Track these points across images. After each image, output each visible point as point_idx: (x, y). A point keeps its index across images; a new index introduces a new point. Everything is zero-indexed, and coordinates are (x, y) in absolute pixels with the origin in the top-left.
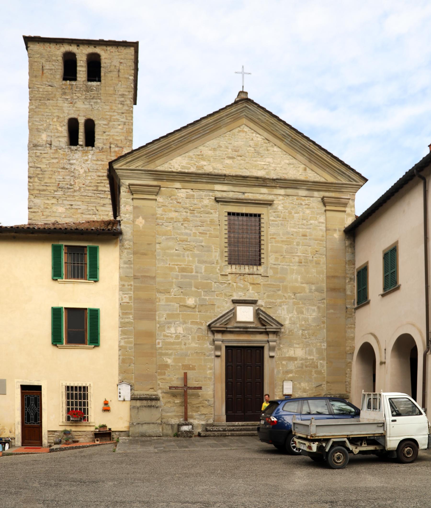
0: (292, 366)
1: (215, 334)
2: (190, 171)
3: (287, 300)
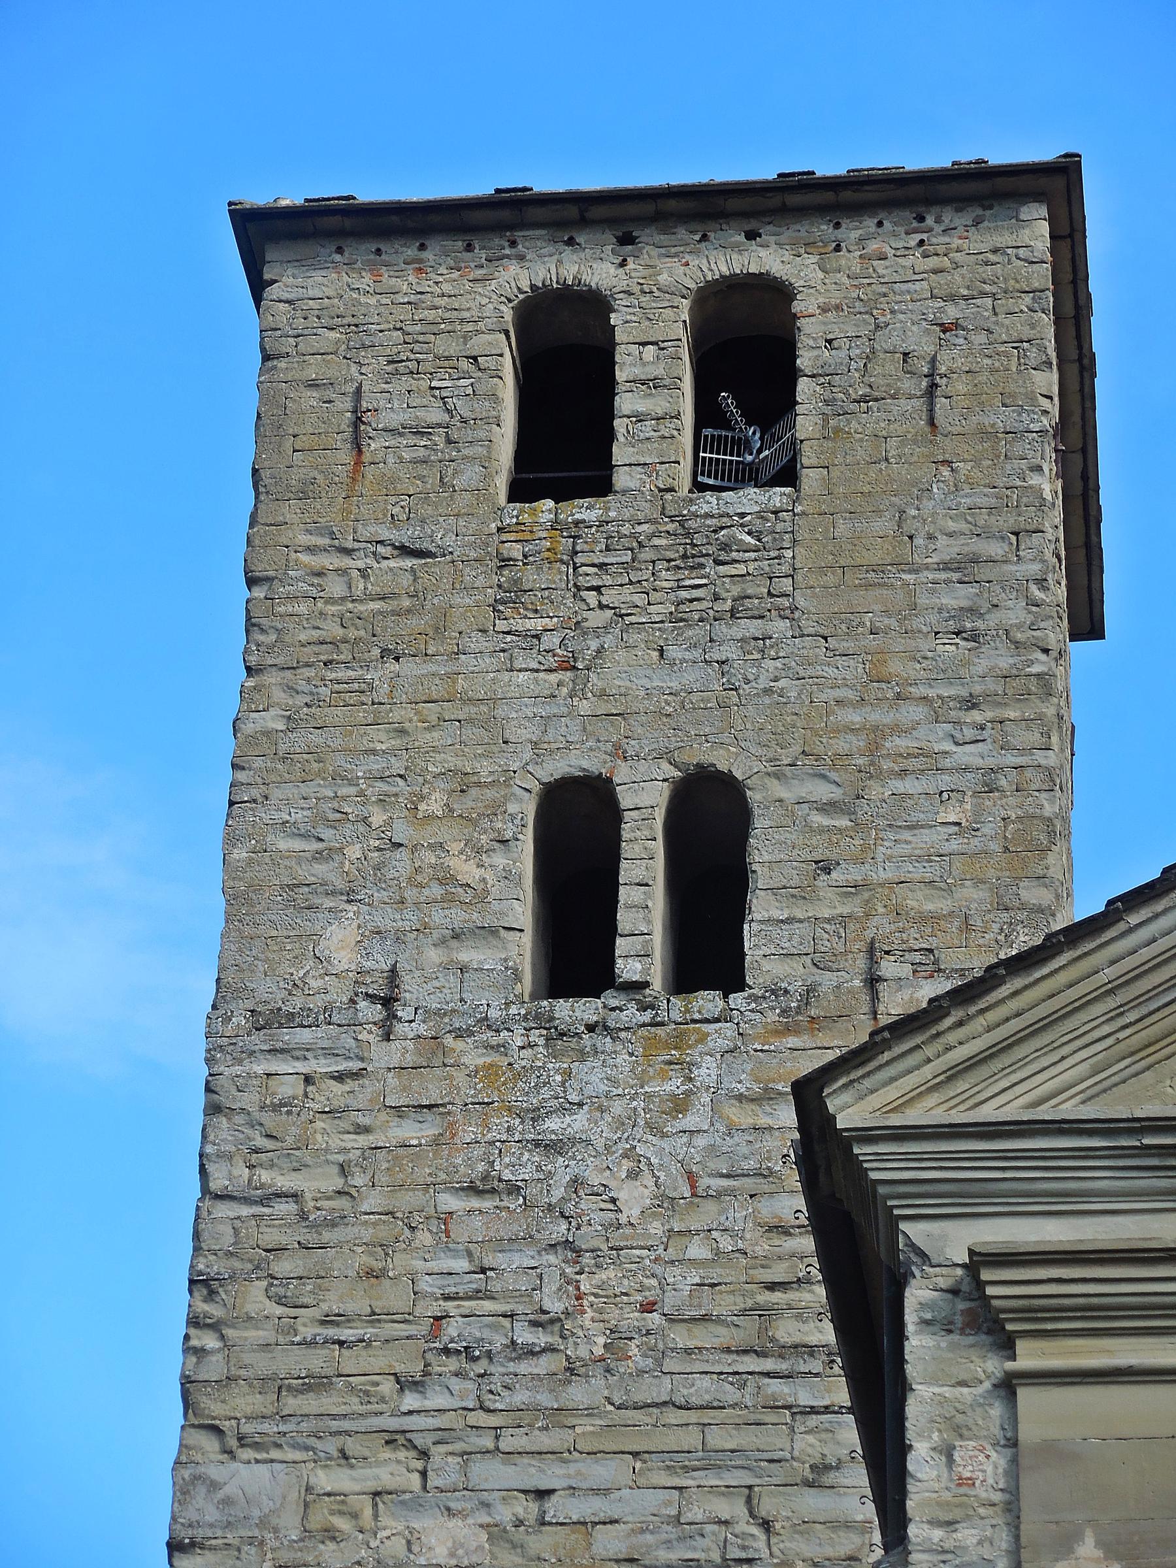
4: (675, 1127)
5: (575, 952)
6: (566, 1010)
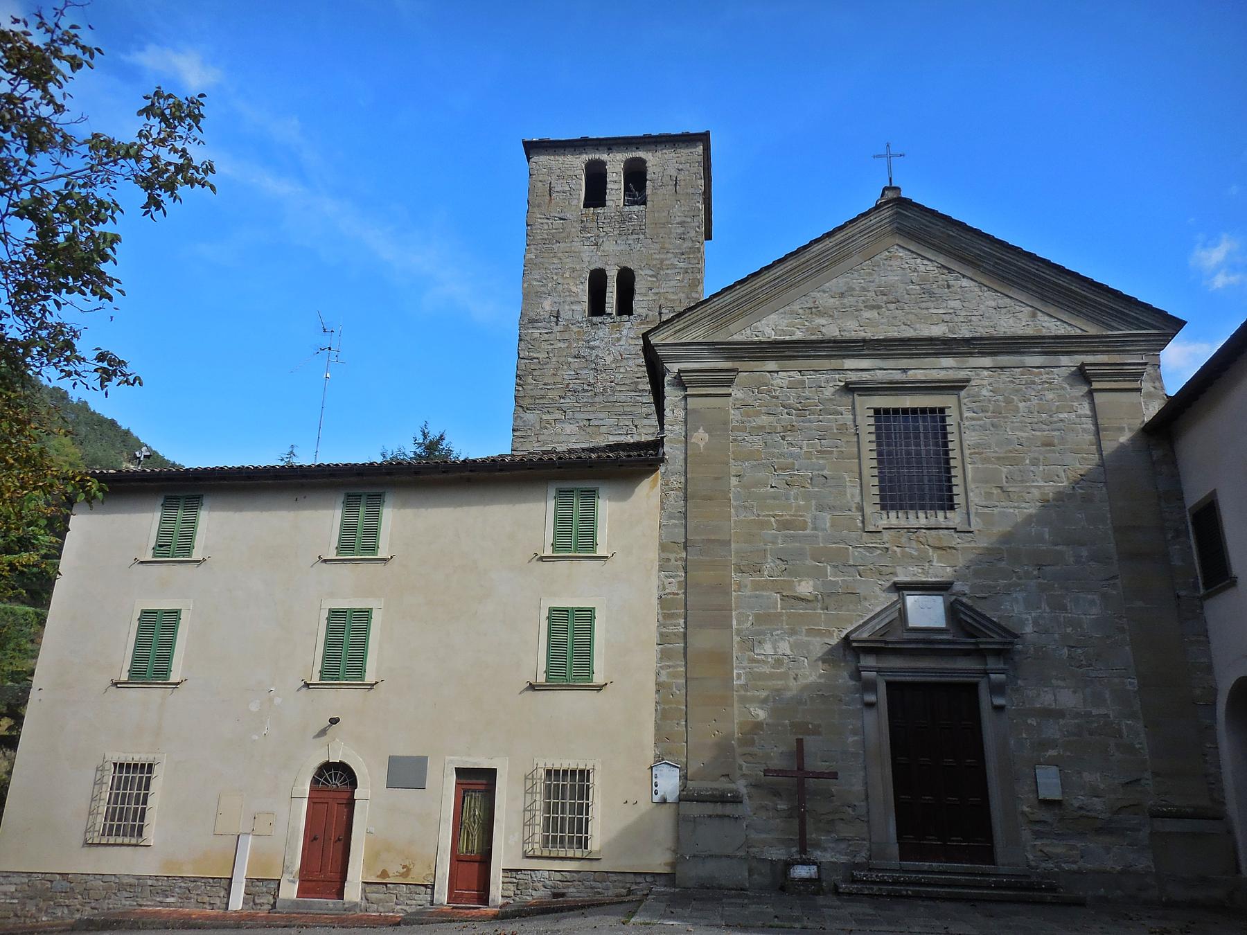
0: (1052, 731)
1: (862, 657)
2: (794, 338)
3: (1023, 581)
4: (619, 342)
5: (597, 306)
6: (594, 319)
